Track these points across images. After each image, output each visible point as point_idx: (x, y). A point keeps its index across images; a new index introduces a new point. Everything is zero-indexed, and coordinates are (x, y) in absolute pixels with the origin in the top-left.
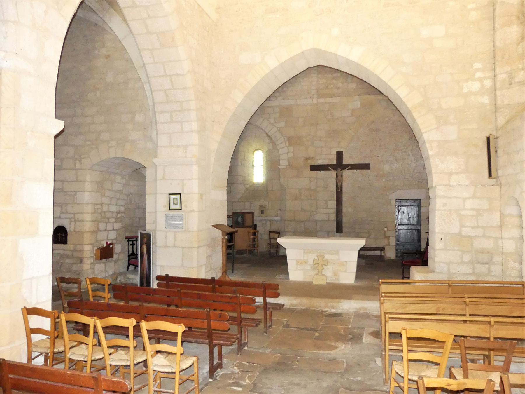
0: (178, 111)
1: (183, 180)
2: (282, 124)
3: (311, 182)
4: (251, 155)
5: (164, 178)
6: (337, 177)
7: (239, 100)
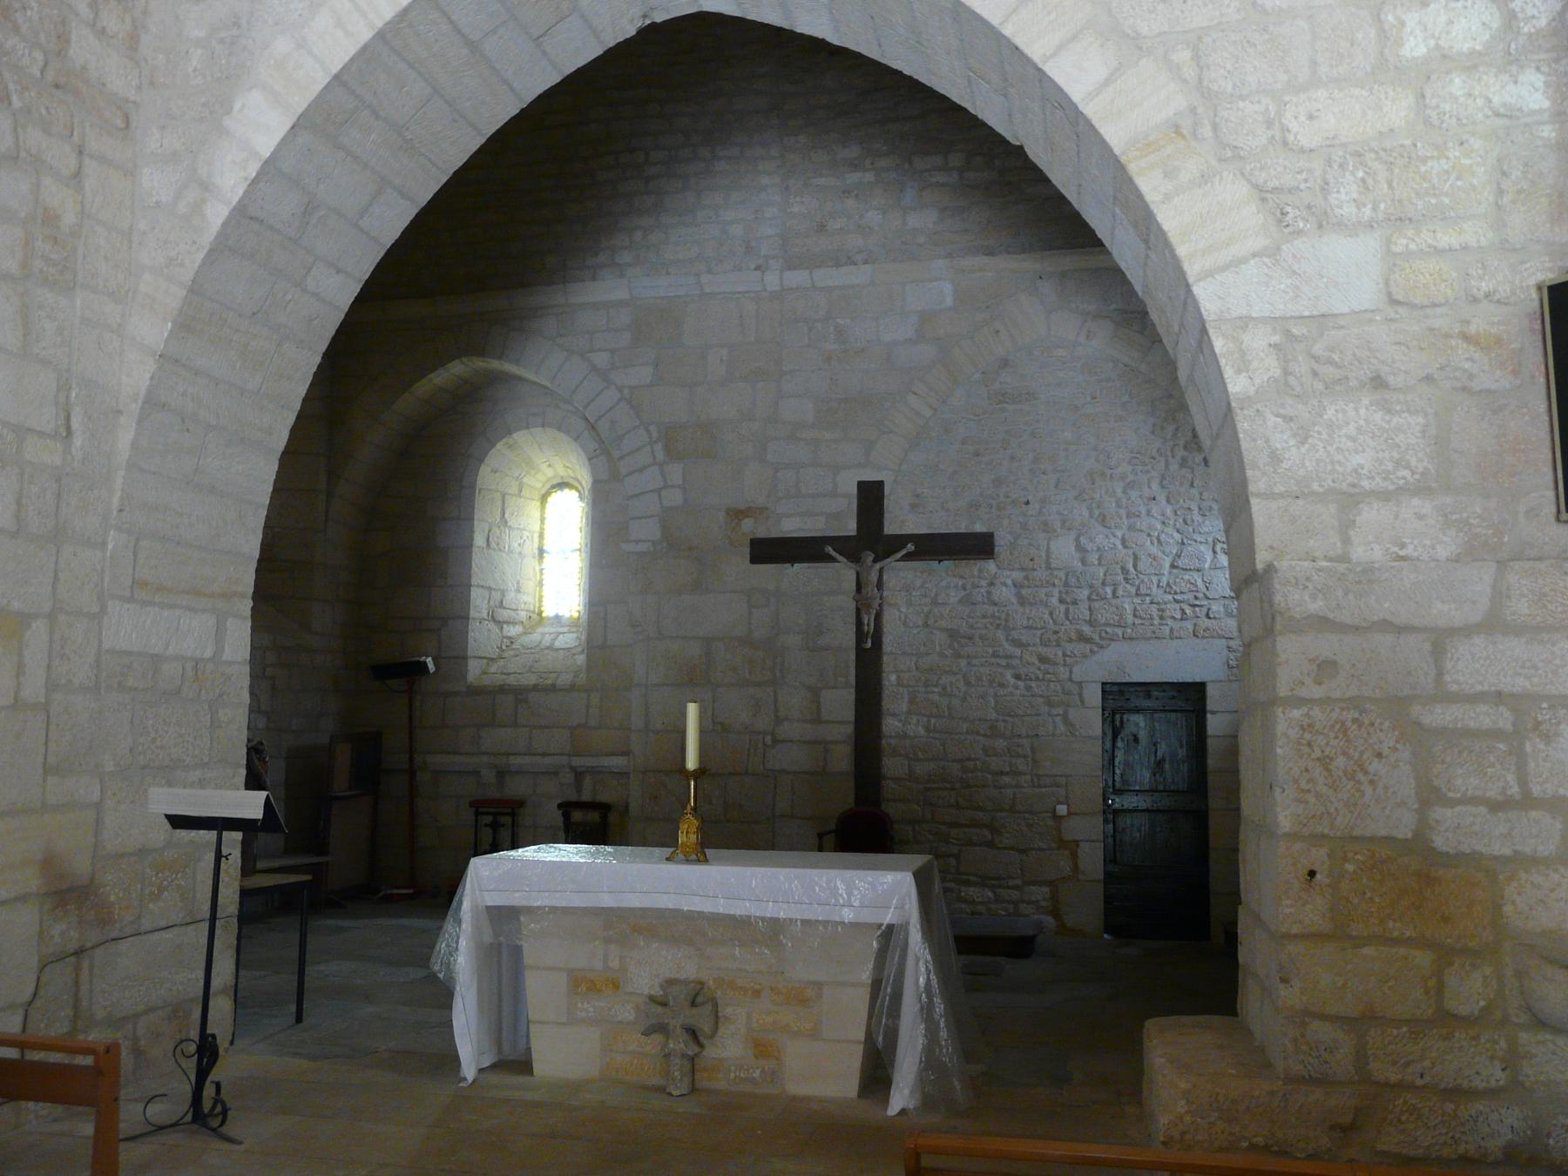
3: (754, 611)
4: (533, 509)
6: (859, 587)
7: (266, 145)
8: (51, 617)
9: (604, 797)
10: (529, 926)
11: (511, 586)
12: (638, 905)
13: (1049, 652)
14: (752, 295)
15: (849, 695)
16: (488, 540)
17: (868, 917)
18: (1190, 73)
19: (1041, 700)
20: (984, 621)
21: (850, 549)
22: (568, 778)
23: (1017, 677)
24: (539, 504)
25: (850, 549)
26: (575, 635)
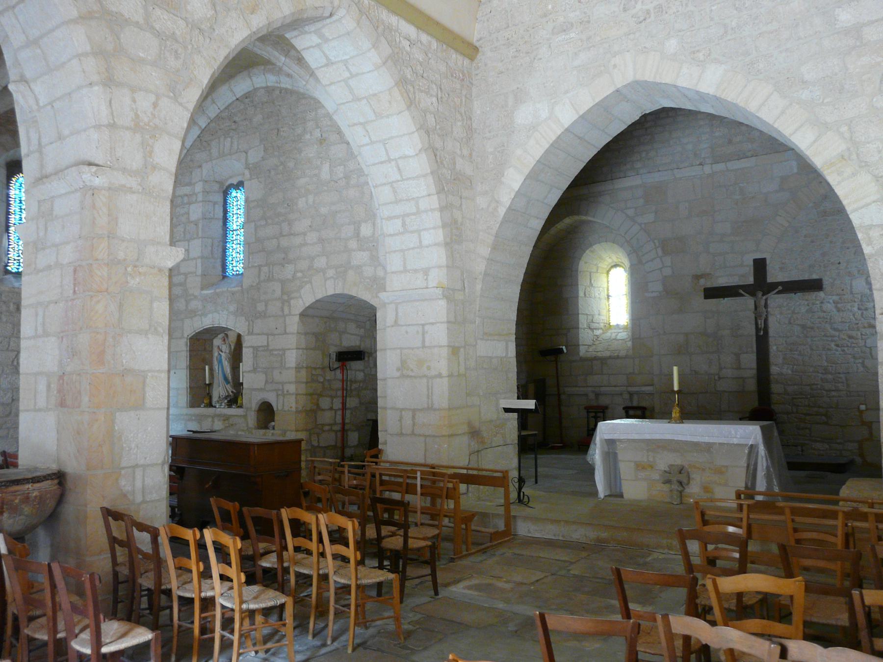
0: (414, 214)
1: (423, 325)
2: (650, 217)
4: (603, 277)
5: (396, 323)
7: (516, 186)
8: (465, 347)
9: (643, 404)
10: (620, 446)
11: (596, 313)
12: (658, 438)
13: (854, 333)
14: (699, 176)
15: (754, 357)
16: (585, 293)
17: (743, 441)
18: (847, 135)
19: (850, 356)
20: (819, 320)
21: (750, 290)
22: (626, 396)
23: (837, 346)
24: (606, 275)
25: (750, 290)
26: (625, 333)
